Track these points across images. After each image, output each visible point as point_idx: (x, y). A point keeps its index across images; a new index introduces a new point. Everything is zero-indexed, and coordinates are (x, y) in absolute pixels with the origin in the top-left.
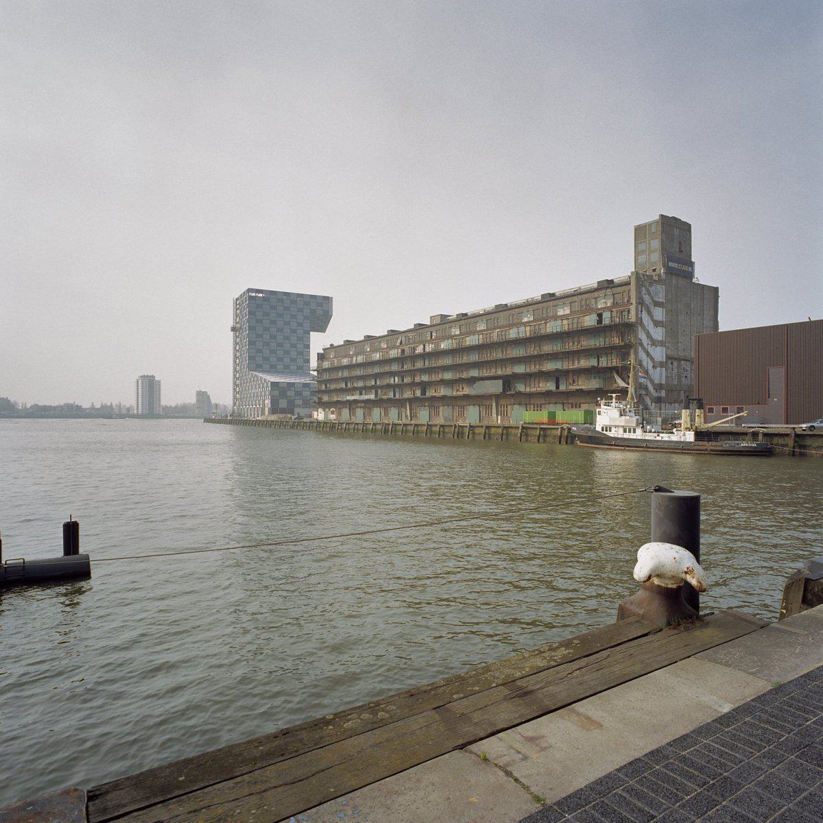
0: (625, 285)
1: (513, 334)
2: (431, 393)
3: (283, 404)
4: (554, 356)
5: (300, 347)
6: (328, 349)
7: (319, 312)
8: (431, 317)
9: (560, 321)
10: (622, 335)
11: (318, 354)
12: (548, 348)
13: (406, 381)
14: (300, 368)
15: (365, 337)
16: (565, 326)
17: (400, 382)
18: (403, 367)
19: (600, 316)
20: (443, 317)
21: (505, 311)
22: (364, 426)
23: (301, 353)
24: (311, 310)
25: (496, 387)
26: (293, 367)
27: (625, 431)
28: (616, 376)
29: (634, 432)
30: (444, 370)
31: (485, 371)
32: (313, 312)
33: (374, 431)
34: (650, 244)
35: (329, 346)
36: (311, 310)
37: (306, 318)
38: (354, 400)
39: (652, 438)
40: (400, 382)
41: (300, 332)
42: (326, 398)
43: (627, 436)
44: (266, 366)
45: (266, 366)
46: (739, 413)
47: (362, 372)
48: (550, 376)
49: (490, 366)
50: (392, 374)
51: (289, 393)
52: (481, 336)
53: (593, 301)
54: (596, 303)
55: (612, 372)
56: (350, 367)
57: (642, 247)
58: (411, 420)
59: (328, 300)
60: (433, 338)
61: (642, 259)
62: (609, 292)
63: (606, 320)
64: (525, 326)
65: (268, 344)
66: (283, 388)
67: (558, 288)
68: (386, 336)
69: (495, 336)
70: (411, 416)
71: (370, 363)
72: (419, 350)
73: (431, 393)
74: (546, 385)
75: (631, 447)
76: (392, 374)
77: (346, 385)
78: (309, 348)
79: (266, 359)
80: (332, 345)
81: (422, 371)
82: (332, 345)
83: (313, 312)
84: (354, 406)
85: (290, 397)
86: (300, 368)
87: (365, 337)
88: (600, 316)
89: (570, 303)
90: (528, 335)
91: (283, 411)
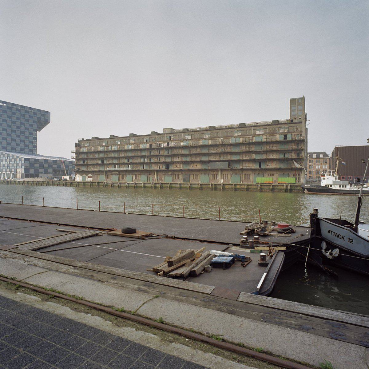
0: (251, 127)
1: (201, 143)
2: (173, 167)
3: (32, 171)
4: (272, 152)
5: (31, 138)
6: (81, 141)
7: (43, 119)
8: (164, 129)
9: (117, 146)
10: (298, 145)
11: (76, 143)
12: (253, 148)
13: (152, 161)
14: (31, 151)
15: (93, 137)
16: (190, 144)
17: (149, 161)
18: (150, 154)
19: (285, 136)
20: (172, 129)
21: (244, 127)
22: (135, 185)
23: (31, 142)
24: (38, 118)
25: (225, 166)
26: (26, 150)
27: (340, 187)
28: (294, 161)
29: (346, 187)
30: (113, 159)
31: (271, 156)
32: (39, 119)
33: (128, 187)
34: (298, 108)
35: (81, 140)
36: (38, 118)
37: (34, 122)
38: (138, 170)
39: (356, 190)
40: (149, 161)
41: (31, 130)
42: (83, 169)
43: (342, 188)
44: (10, 148)
45: (18, 149)
46: (66, 170)
47: (239, 150)
48: (256, 161)
49: (226, 155)
50: (144, 157)
51: (36, 165)
52: (119, 147)
53: (277, 129)
54: (279, 130)
55: (292, 161)
56: (224, 145)
57: (293, 108)
58: (157, 181)
59: (47, 113)
60: (172, 140)
61: (293, 113)
62: (134, 138)
63: (289, 137)
64: (104, 147)
65: (28, 129)
66: (42, 163)
67: (190, 127)
68: (129, 137)
69: (93, 149)
70: (157, 179)
71: (178, 147)
72: (164, 145)
73: (173, 167)
74: (253, 165)
75: (346, 193)
76: (144, 157)
77: (128, 161)
78: (36, 139)
79: (9, 144)
80: (83, 139)
81: (166, 156)
82: (83, 139)
83: (39, 119)
84: (109, 173)
85: (46, 167)
86: (31, 151)
87: (93, 137)
88: (285, 136)
89: (191, 135)
90: (209, 144)
91: (32, 176)
